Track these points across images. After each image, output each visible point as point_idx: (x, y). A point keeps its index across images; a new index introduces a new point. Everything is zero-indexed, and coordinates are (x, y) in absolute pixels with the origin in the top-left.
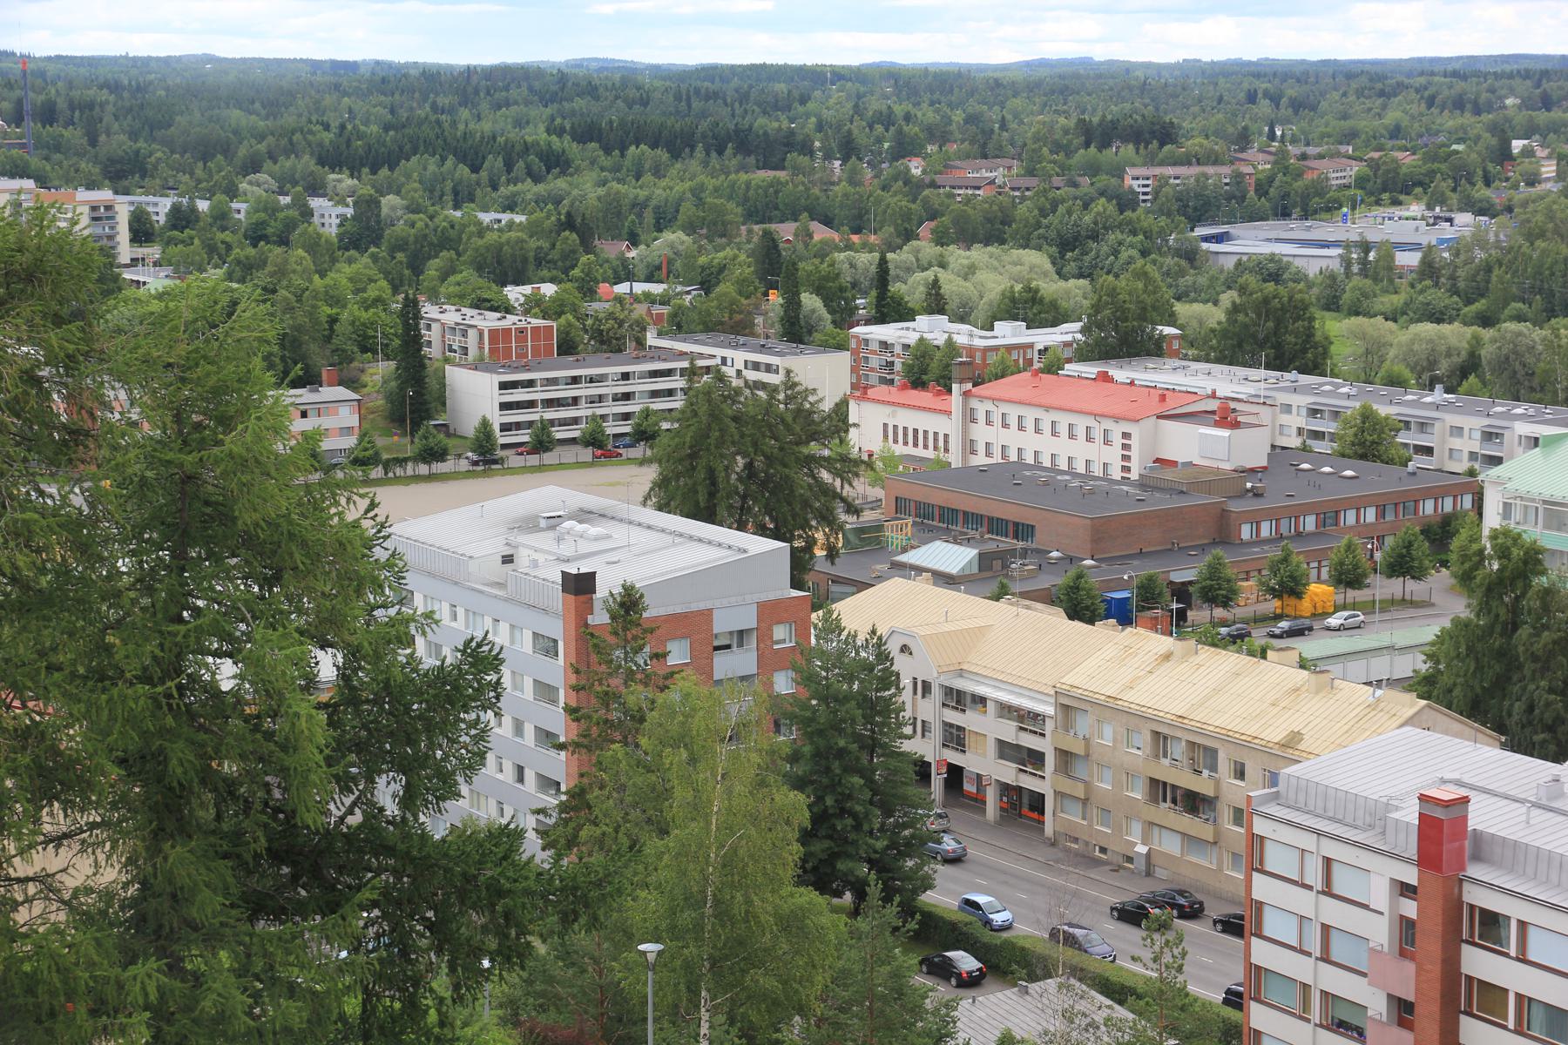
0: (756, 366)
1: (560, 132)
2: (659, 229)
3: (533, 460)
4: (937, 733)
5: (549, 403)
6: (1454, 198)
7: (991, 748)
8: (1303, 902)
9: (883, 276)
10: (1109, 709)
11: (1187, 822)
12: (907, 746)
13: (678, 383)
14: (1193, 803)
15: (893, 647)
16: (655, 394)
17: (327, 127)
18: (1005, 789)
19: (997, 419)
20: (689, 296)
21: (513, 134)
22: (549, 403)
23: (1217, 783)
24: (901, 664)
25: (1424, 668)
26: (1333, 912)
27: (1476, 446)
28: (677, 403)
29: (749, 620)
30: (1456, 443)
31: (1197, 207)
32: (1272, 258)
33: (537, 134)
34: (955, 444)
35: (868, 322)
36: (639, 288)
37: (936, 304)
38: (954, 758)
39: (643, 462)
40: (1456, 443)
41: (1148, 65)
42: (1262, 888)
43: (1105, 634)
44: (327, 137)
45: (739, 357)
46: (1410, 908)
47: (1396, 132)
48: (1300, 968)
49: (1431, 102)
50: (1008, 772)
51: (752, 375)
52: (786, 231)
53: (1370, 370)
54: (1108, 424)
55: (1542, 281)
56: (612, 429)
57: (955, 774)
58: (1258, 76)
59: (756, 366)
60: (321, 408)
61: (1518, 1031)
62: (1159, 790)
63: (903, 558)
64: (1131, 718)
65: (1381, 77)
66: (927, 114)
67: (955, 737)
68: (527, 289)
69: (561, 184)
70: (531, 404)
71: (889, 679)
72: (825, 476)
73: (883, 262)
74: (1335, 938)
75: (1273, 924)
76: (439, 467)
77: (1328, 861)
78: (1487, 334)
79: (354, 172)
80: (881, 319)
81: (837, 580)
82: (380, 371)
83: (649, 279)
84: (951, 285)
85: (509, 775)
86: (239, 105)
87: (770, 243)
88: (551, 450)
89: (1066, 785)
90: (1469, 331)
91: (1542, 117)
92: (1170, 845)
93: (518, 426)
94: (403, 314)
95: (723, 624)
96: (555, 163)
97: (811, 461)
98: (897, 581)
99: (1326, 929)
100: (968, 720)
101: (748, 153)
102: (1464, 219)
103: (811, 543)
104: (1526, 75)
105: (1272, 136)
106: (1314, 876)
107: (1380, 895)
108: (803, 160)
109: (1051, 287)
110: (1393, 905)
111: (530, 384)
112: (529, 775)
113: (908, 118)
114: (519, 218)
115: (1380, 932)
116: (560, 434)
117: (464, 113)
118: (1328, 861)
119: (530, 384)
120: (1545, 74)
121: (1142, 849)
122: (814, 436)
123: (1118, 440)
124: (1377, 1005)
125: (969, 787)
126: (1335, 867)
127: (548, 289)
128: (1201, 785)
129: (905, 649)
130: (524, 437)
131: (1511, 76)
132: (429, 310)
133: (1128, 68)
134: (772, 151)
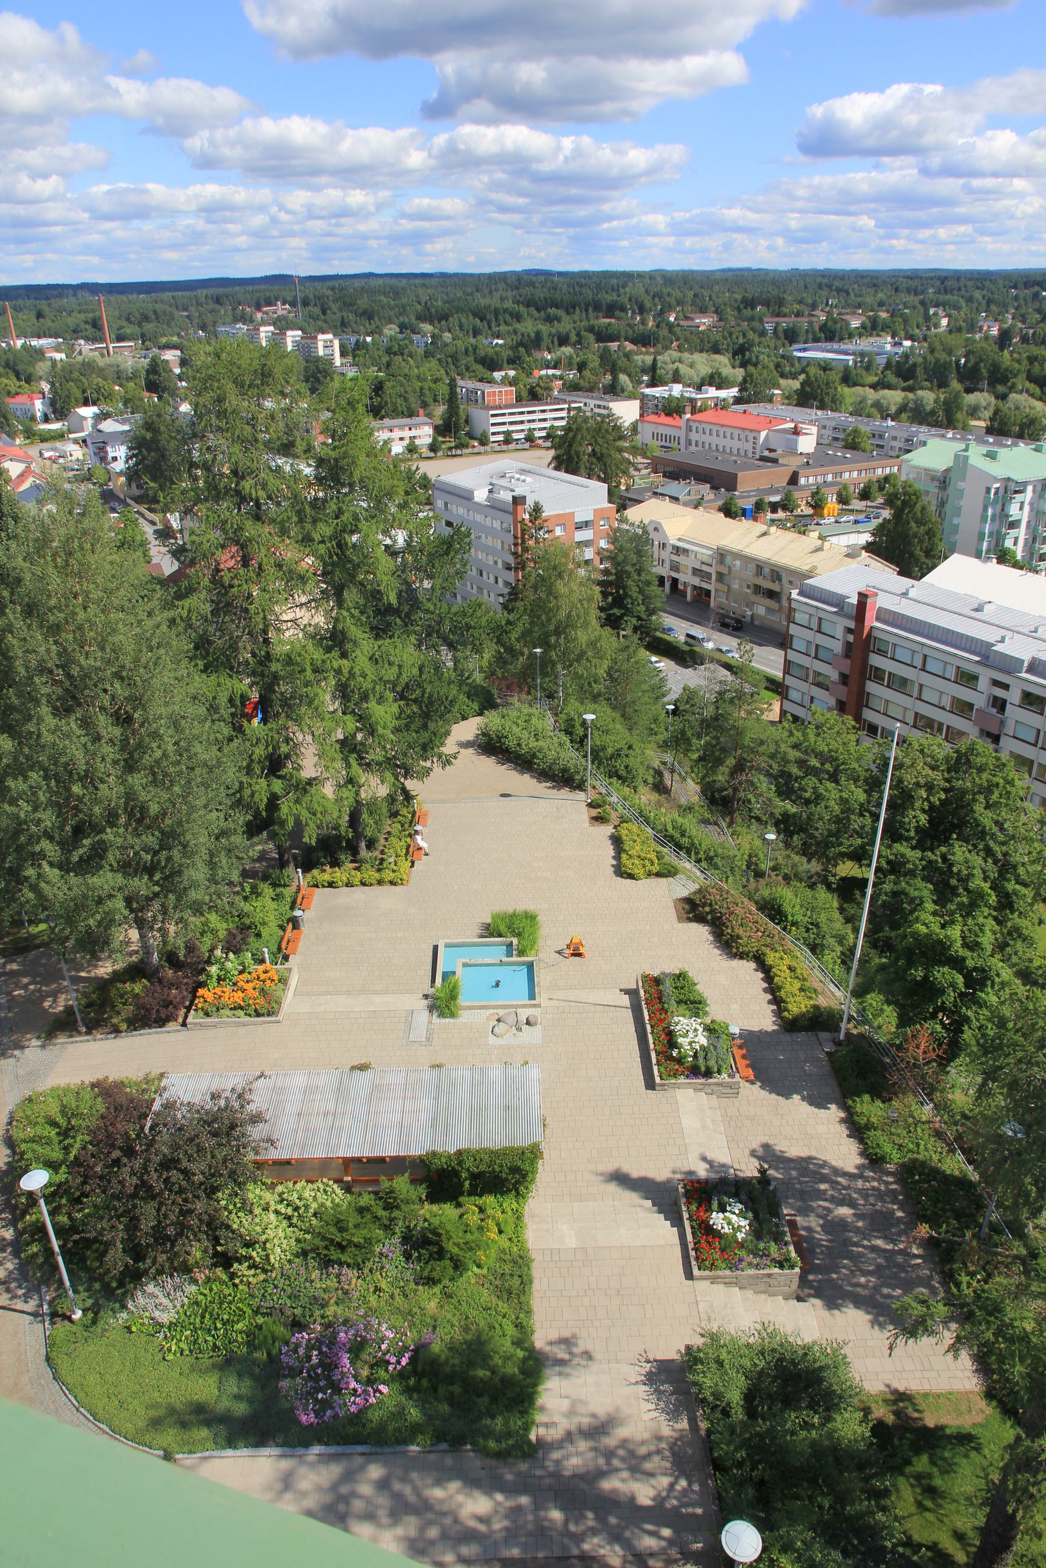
0: (599, 407)
1: (518, 303)
2: (560, 345)
3: (504, 447)
4: (667, 565)
5: (511, 423)
6: (902, 334)
7: (690, 571)
8: (809, 635)
9: (654, 367)
10: (738, 556)
11: (769, 602)
12: (654, 570)
13: (564, 414)
14: (772, 595)
15: (650, 529)
16: (555, 419)
17: (420, 303)
18: (695, 587)
19: (700, 430)
20: (572, 375)
21: (498, 305)
22: (511, 423)
23: (782, 586)
24: (653, 535)
25: (871, 539)
26: (821, 640)
27: (901, 445)
28: (563, 423)
29: (590, 517)
30: (894, 443)
31: (791, 336)
32: (825, 360)
33: (509, 304)
34: (683, 441)
35: (648, 386)
36: (550, 372)
37: (676, 378)
38: (675, 575)
39: (548, 448)
40: (894, 443)
41: (775, 271)
42: (793, 629)
43: (744, 526)
44: (419, 307)
45: (592, 403)
46: (851, 638)
47: (881, 304)
48: (805, 661)
49: (897, 290)
50: (696, 581)
51: (597, 410)
52: (614, 346)
53: (858, 411)
54: (747, 433)
55: (480, 589)
56: (537, 434)
57: (675, 582)
58: (823, 276)
59: (599, 407)
60: (417, 426)
61: (888, 686)
62: (757, 589)
63: (659, 491)
64: (747, 559)
65: (877, 278)
66: (678, 294)
67: (675, 567)
68: (503, 373)
69: (518, 326)
70: (504, 424)
71: (649, 542)
72: (626, 455)
73: (655, 360)
74: (820, 650)
75: (797, 644)
76: (465, 451)
77: (820, 619)
78: (911, 396)
79: (431, 323)
80: (653, 384)
81: (630, 499)
82: (440, 410)
83: (555, 367)
84: (684, 369)
85: (492, 580)
86: (384, 294)
87: (606, 350)
88: (687, 667)
89: (720, 586)
90: (903, 394)
91: (943, 297)
92: (761, 611)
93: (499, 433)
94: (450, 385)
95: (579, 518)
96: (518, 317)
97: (620, 450)
98: (653, 500)
99: (817, 646)
100: (681, 559)
101: (600, 310)
102: (907, 343)
103: (619, 483)
104: (939, 278)
105: (827, 304)
106: (918, 663)
107: (839, 633)
108: (622, 314)
109: (727, 371)
110: (844, 637)
111: (503, 415)
112: (500, 581)
113: (669, 295)
114: (501, 342)
115: (838, 647)
116: (515, 436)
117: (478, 295)
118: (820, 619)
119: (503, 415)
120: (946, 278)
121: (749, 613)
122: (622, 438)
123: (751, 440)
124: (834, 676)
125: (681, 587)
126: (928, 660)
127: (512, 373)
128: (775, 587)
129: (656, 529)
130: (501, 438)
131: (932, 279)
132: (460, 383)
133: (766, 272)
134: (611, 310)
